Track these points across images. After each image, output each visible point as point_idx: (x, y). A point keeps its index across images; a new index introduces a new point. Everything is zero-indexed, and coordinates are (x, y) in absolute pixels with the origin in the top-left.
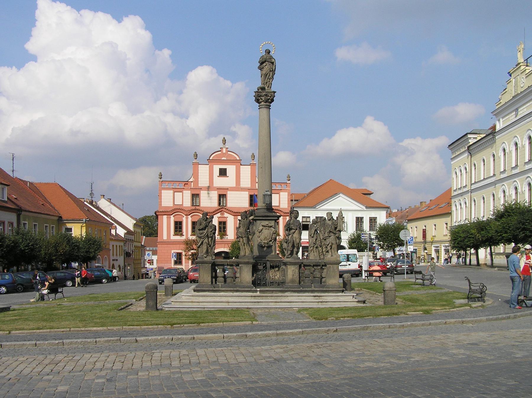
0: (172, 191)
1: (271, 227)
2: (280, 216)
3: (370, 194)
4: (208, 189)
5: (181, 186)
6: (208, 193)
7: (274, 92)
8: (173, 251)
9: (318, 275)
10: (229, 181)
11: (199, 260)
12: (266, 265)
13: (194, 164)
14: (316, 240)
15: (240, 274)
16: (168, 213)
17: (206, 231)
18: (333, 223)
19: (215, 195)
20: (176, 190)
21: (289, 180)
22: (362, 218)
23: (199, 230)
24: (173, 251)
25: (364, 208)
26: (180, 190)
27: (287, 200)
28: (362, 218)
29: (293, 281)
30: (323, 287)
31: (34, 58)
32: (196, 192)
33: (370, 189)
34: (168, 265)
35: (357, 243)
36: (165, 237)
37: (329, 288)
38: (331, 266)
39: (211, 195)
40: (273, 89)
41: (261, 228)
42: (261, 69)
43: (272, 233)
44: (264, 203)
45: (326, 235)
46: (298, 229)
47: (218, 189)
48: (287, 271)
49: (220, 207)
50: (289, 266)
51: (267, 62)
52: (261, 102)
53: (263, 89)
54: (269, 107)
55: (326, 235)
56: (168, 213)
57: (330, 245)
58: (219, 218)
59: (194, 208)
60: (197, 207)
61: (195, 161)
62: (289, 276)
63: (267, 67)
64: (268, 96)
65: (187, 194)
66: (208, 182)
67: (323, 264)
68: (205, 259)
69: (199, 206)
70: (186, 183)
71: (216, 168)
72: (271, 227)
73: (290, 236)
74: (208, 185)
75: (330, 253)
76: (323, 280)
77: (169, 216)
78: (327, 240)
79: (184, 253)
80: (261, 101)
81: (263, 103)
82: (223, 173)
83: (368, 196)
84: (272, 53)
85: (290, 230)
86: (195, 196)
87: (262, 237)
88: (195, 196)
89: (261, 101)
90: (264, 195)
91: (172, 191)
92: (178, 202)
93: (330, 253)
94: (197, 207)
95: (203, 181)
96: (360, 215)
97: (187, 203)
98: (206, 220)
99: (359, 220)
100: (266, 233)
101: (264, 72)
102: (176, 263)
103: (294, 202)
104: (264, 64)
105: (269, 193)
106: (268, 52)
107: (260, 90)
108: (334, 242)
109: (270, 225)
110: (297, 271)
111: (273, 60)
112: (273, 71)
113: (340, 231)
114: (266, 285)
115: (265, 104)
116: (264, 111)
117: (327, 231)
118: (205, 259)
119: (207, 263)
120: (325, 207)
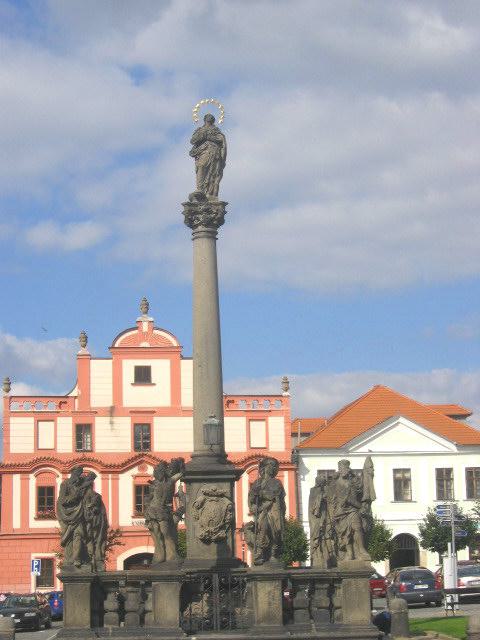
0: (31, 420)
1: (222, 495)
2: (242, 472)
3: (464, 416)
4: (112, 412)
5: (52, 406)
6: (112, 423)
7: (224, 204)
8: (34, 556)
9: (325, 603)
10: (155, 395)
11: (327, 585)
12: (210, 583)
13: (80, 357)
14: (325, 522)
15: (154, 603)
16: (24, 468)
17: (77, 509)
18: (352, 485)
19: (125, 426)
20: (41, 417)
21: (286, 390)
22: (449, 471)
23: (65, 505)
24: (34, 556)
25: (454, 449)
26: (50, 417)
27: (283, 433)
28: (449, 471)
29: (269, 617)
30: (336, 629)
31: (183, 205)
32: (83, 420)
33: (466, 406)
34: (24, 586)
35: (463, 533)
36: (17, 524)
37: (348, 630)
38: (352, 581)
39: (115, 426)
40: (221, 198)
41: (201, 498)
42: (195, 155)
43: (225, 508)
44: (206, 443)
45: (340, 510)
46: (277, 499)
47: (134, 412)
48: (257, 596)
49: (137, 454)
50: (259, 584)
51: (207, 142)
52: (196, 226)
53: (200, 197)
54: (213, 236)
55: (340, 510)
56: (24, 468)
57: (348, 533)
58: (135, 477)
59: (80, 455)
60: (88, 455)
61: (82, 351)
62: (260, 605)
63: (208, 152)
64: (211, 212)
65: (66, 426)
66: (111, 398)
67: (335, 576)
68: (78, 571)
69: (91, 451)
70: (63, 401)
71: (129, 366)
72: (222, 495)
73: (261, 515)
74: (110, 404)
75: (349, 552)
76: (337, 613)
77: (25, 476)
78: (342, 523)
79: (58, 561)
80: (196, 222)
81: (200, 228)
82: (143, 376)
83: (462, 422)
84: (219, 122)
85: (260, 504)
86: (83, 431)
87: (204, 519)
88: (83, 431)
89: (196, 222)
90: (206, 426)
91: (31, 420)
92: (46, 442)
93: (349, 552)
94: (88, 455)
95: (101, 394)
96: (444, 463)
97: (66, 445)
98: (79, 484)
99: (444, 477)
100: (212, 508)
101: (202, 162)
102: (39, 582)
103: (300, 439)
104: (203, 146)
105: (216, 421)
106: (211, 120)
107: (195, 201)
108: (356, 527)
109: (220, 491)
110: (278, 593)
111: (220, 138)
112: (220, 161)
113: (369, 502)
114: (212, 628)
115: (205, 229)
116: (204, 244)
117: (341, 501)
118: (78, 571)
119: (82, 581)
120: (364, 449)
